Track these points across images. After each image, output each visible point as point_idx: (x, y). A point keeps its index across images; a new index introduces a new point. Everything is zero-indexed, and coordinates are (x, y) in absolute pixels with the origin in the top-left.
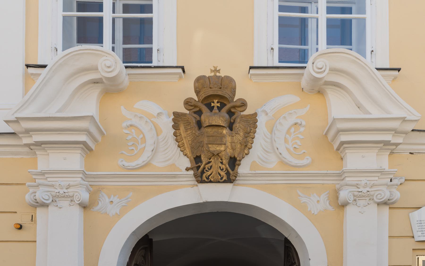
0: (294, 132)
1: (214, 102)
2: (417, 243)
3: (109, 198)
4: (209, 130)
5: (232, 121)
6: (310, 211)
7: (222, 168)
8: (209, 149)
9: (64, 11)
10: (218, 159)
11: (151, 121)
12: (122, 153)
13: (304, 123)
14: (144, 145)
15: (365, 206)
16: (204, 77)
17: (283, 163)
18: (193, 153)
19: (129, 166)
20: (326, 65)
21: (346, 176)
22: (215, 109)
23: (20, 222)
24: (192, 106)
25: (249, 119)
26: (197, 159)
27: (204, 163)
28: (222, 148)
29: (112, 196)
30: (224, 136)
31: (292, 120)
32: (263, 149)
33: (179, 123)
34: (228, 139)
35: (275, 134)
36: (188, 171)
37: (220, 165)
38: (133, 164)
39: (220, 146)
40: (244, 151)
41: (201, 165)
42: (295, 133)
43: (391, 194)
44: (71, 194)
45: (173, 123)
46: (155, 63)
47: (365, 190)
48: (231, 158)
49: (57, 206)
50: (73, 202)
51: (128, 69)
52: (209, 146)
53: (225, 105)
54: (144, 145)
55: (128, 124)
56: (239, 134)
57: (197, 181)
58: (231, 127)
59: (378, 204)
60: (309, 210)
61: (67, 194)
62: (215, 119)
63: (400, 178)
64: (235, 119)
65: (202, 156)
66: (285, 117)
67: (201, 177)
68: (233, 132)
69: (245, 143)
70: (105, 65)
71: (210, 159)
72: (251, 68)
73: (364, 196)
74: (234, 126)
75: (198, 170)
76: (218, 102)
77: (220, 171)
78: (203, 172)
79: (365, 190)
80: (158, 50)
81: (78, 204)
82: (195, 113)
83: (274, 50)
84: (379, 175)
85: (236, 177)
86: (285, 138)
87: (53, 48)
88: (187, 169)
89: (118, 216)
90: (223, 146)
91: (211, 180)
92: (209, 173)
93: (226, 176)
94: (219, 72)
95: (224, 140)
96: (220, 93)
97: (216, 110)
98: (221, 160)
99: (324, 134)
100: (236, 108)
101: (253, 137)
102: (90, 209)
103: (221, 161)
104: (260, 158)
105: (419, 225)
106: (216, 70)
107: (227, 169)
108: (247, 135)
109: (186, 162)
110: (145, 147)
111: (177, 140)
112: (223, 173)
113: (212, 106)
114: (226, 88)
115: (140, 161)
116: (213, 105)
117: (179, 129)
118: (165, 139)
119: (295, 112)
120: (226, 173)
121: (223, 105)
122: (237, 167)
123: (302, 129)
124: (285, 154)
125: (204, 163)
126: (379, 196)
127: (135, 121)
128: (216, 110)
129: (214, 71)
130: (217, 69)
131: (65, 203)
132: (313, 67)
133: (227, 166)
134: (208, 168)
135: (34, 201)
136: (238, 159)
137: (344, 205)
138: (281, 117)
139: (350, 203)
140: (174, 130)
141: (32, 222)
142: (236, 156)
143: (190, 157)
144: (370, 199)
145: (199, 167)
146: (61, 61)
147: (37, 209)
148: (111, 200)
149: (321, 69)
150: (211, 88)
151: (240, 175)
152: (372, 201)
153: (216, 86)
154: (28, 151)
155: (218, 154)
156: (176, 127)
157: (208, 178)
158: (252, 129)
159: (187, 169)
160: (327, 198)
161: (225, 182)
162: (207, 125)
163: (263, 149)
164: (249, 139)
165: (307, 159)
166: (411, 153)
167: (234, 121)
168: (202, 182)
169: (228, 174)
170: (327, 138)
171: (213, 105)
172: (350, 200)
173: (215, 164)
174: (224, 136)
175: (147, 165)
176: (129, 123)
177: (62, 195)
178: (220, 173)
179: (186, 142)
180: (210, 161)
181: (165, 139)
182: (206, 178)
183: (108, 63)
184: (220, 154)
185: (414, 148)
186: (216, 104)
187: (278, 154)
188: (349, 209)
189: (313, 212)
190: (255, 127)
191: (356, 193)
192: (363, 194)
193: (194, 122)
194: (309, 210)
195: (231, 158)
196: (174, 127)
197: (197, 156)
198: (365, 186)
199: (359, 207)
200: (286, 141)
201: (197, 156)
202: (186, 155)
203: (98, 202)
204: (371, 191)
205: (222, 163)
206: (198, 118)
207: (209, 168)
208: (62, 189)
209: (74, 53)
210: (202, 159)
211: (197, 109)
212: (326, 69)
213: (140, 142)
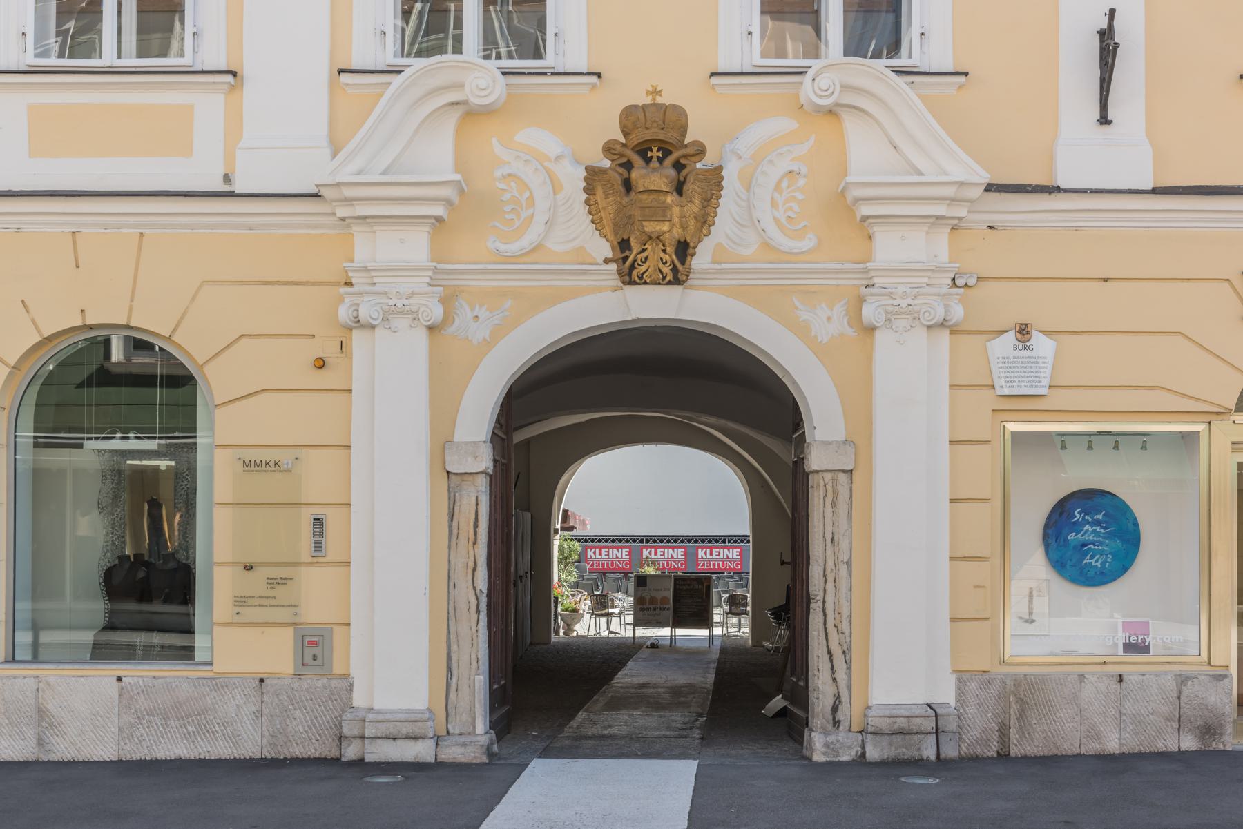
0: (788, 187)
1: (651, 151)
2: (1001, 399)
3: (473, 309)
4: (644, 197)
6: (816, 337)
7: (664, 261)
8: (643, 229)
10: (657, 245)
13: (804, 170)
14: (531, 211)
15: (906, 331)
16: (636, 106)
17: (767, 245)
18: (616, 234)
19: (506, 252)
21: (873, 275)
22: (654, 161)
24: (615, 154)
25: (710, 177)
26: (624, 245)
27: (635, 252)
28: (665, 227)
29: (477, 308)
31: (784, 165)
32: (735, 220)
34: (676, 211)
35: (754, 194)
36: (607, 264)
37: (662, 255)
39: (661, 223)
40: (701, 232)
41: (631, 255)
42: (789, 190)
44: (414, 309)
45: (585, 184)
47: (904, 304)
48: (679, 242)
49: (390, 328)
50: (416, 322)
51: (507, 76)
52: (644, 223)
53: (670, 153)
54: (531, 211)
57: (623, 283)
58: (679, 189)
59: (929, 327)
60: (813, 334)
61: (407, 308)
62: (654, 181)
63: (968, 276)
64: (687, 175)
65: (631, 239)
66: (771, 162)
67: (630, 274)
69: (703, 217)
70: (477, 86)
71: (645, 245)
72: (712, 75)
75: (624, 263)
76: (658, 151)
77: (661, 265)
78: (632, 267)
79: (904, 304)
80: (556, 35)
82: (621, 165)
83: (753, 34)
84: (929, 274)
85: (688, 276)
86: (772, 198)
87: (378, 32)
88: (606, 261)
89: (489, 344)
90: (667, 223)
91: (645, 281)
92: (643, 269)
93: (672, 274)
95: (669, 214)
96: (661, 137)
98: (664, 246)
99: (839, 190)
100: (689, 158)
101: (715, 206)
102: (440, 331)
103: (663, 248)
105: (1001, 365)
106: (656, 92)
107: (673, 262)
108: (705, 204)
109: (604, 249)
111: (590, 212)
112: (666, 270)
113: (649, 156)
114: (671, 128)
115: (524, 243)
116: (650, 154)
117: (595, 194)
118: (567, 202)
120: (671, 270)
121: (667, 153)
122: (689, 258)
123: (801, 182)
124: (774, 232)
125: (635, 252)
126: (927, 314)
128: (654, 163)
129: (652, 93)
130: (658, 90)
131: (401, 323)
132: (813, 86)
133: (674, 257)
134: (641, 260)
135: (354, 319)
136: (691, 245)
137: (871, 329)
139: (878, 327)
140: (586, 196)
141: (342, 355)
142: (688, 240)
143: (612, 241)
144: (914, 319)
146: (407, 82)
147: (355, 332)
148: (475, 314)
149: (827, 90)
150: (647, 128)
151: (695, 271)
153: (655, 125)
154: (336, 222)
156: (589, 190)
157: (641, 278)
158: (714, 194)
159: (606, 261)
160: (844, 312)
161: (669, 283)
162: (641, 190)
163: (735, 220)
164: (710, 210)
165: (810, 239)
166: (990, 227)
167: (685, 179)
168: (632, 283)
169: (675, 270)
170: (845, 197)
171: (650, 154)
172: (877, 322)
173: (654, 253)
175: (538, 248)
176: (506, 171)
177: (400, 311)
178: (661, 268)
179: (608, 214)
180: (645, 248)
181: (567, 202)
182: (638, 277)
183: (482, 83)
185: (994, 219)
186: (655, 153)
187: (761, 231)
188: (878, 335)
190: (720, 188)
191: (890, 309)
192: (902, 310)
193: (620, 182)
194: (813, 334)
195: (679, 242)
196: (586, 190)
197: (623, 239)
199: (896, 332)
200: (774, 204)
201: (623, 239)
202: (605, 237)
203: (454, 318)
204: (915, 305)
205: (664, 251)
206: (626, 175)
207: (643, 260)
208: (400, 299)
209: (428, 68)
210: (632, 244)
211: (624, 160)
212: (834, 90)
213: (524, 205)
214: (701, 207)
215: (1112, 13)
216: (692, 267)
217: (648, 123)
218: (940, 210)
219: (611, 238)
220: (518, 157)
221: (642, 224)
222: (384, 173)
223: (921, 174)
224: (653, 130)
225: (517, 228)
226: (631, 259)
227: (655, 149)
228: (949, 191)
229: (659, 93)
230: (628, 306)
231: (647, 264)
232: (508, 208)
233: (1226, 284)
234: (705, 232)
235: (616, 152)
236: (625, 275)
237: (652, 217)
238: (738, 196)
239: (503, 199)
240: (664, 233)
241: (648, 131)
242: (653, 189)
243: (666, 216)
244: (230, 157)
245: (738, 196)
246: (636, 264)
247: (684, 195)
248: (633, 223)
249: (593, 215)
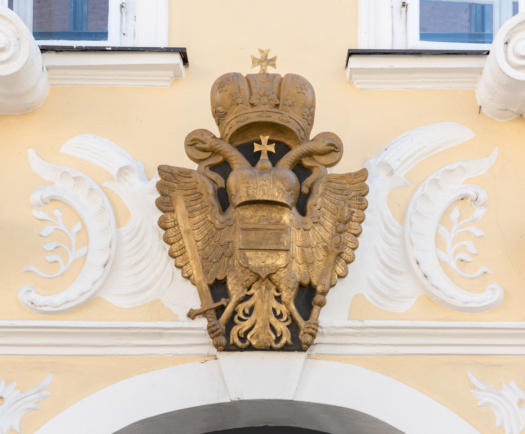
0: (460, 219)
1: (259, 142)
4: (248, 212)
5: (305, 190)
7: (278, 313)
8: (247, 262)
10: (268, 289)
11: (101, 187)
12: (29, 271)
13: (483, 196)
14: (82, 251)
18: (206, 272)
19: (46, 306)
22: (263, 159)
24: (204, 150)
25: (348, 186)
27: (234, 299)
28: (280, 261)
30: (283, 230)
32: (382, 262)
33: (173, 194)
35: (411, 224)
37: (275, 304)
39: (274, 254)
41: (228, 303)
45: (158, 195)
48: (301, 286)
51: (47, 55)
52: (248, 254)
53: (288, 149)
54: (82, 251)
56: (321, 224)
60: (498, 424)
62: (263, 185)
64: (312, 184)
65: (229, 280)
66: (435, 182)
68: (307, 219)
69: (338, 248)
71: (249, 289)
72: (352, 53)
74: (310, 203)
75: (218, 317)
76: (270, 142)
77: (273, 320)
78: (230, 323)
80: (122, 6)
83: (409, 6)
85: (313, 336)
88: (192, 315)
90: (283, 255)
91: (250, 344)
92: (246, 325)
94: (274, 65)
95: (285, 239)
96: (275, 118)
97: (264, 161)
98: (278, 291)
100: (316, 157)
101: (356, 232)
103: (277, 294)
107: (291, 315)
108: (341, 227)
110: (86, 255)
111: (166, 240)
112: (281, 326)
113: (255, 150)
116: (257, 148)
117: (173, 211)
119: (461, 167)
120: (288, 326)
122: (316, 309)
123: (479, 213)
125: (234, 299)
128: (264, 161)
129: (260, 62)
132: (506, 52)
133: (293, 307)
134: (244, 311)
136: (319, 288)
140: (161, 214)
142: (314, 282)
143: (200, 283)
150: (252, 105)
151: (324, 330)
153: (265, 100)
155: (269, 277)
157: (243, 339)
158: (353, 212)
159: (192, 315)
161: (286, 348)
162: (243, 200)
163: (382, 262)
164: (347, 237)
165: (494, 289)
169: (294, 327)
171: (257, 148)
173: (263, 301)
174: (283, 230)
176: (47, 193)
178: (274, 324)
180: (249, 293)
182: (240, 338)
184: (274, 277)
187: (421, 276)
194: (498, 424)
195: (301, 286)
196: (161, 204)
197: (216, 280)
200: (439, 242)
201: (216, 280)
202: (188, 278)
205: (278, 299)
206: (221, 183)
207: (247, 311)
210: (230, 287)
211: (218, 159)
213: (74, 242)
214: (334, 233)
216: (320, 324)
217: (253, 98)
219: (198, 276)
220: (64, 174)
221: (245, 254)
224: (261, 108)
225: (62, 275)
226: (229, 309)
227: (264, 139)
229: (272, 62)
230: (224, 382)
231: (253, 317)
232: (50, 246)
234: (339, 270)
235: (206, 146)
236: (220, 334)
237: (261, 244)
238: (388, 229)
239: (42, 233)
240: (278, 269)
241: (254, 109)
242: (261, 198)
243: (282, 243)
245: (388, 229)
246: (236, 318)
247: (308, 212)
248: (232, 255)
249: (171, 244)
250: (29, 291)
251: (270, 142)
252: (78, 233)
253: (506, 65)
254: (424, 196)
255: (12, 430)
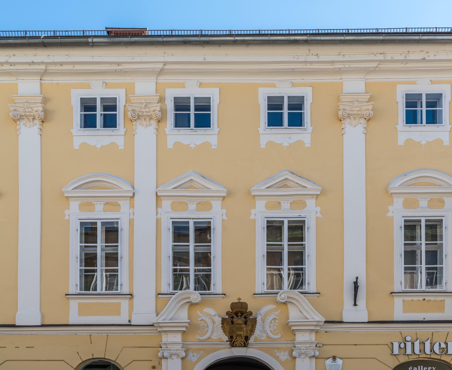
1: (239, 314)
3: (193, 354)
5: (246, 321)
6: (281, 360)
9: (96, 114)
10: (240, 337)
11: (210, 317)
12: (198, 333)
13: (278, 318)
17: (268, 337)
18: (229, 334)
20: (285, 297)
23: (154, 365)
24: (229, 315)
26: (231, 337)
27: (234, 339)
28: (242, 333)
30: (243, 328)
31: (273, 317)
33: (224, 322)
34: (245, 329)
35: (265, 324)
37: (241, 340)
38: (203, 338)
43: (314, 353)
44: (178, 354)
46: (212, 291)
52: (237, 332)
53: (243, 314)
55: (201, 319)
56: (249, 326)
58: (246, 323)
59: (310, 357)
60: (280, 359)
61: (176, 353)
65: (233, 336)
66: (269, 316)
68: (247, 326)
69: (252, 330)
70: (194, 298)
72: (254, 294)
73: (303, 354)
74: (247, 323)
77: (241, 342)
78: (234, 343)
81: (181, 358)
82: (231, 317)
84: (310, 344)
88: (227, 341)
90: (243, 332)
92: (236, 343)
94: (241, 300)
97: (239, 317)
98: (242, 337)
99: (287, 323)
104: (258, 335)
106: (239, 299)
107: (244, 341)
109: (226, 338)
110: (208, 330)
111: (223, 329)
112: (242, 343)
115: (206, 337)
116: (238, 315)
118: (217, 326)
119: (274, 313)
122: (248, 341)
123: (277, 321)
126: (309, 354)
127: (204, 318)
128: (239, 317)
133: (244, 340)
136: (249, 337)
137: (295, 358)
138: (268, 316)
142: (248, 336)
145: (232, 341)
148: (193, 355)
152: (307, 356)
155: (240, 335)
157: (236, 345)
159: (227, 341)
161: (243, 347)
164: (253, 328)
165: (279, 335)
166: (326, 332)
167: (247, 320)
168: (233, 347)
169: (244, 343)
174: (243, 328)
175: (209, 338)
181: (217, 326)
183: (195, 297)
184: (241, 335)
185: (327, 330)
189: (282, 360)
191: (300, 353)
193: (230, 322)
194: (280, 359)
195: (246, 336)
196: (222, 324)
198: (304, 349)
200: (270, 326)
204: (306, 352)
205: (242, 339)
210: (234, 337)
211: (231, 316)
213: (206, 327)
215: (357, 278)
218: (313, 328)
222: (170, 320)
223: (308, 319)
227: (239, 313)
228: (315, 323)
229: (241, 299)
231: (237, 342)
232: (202, 328)
233: (387, 346)
238: (261, 324)
240: (242, 334)
244: (130, 315)
245: (261, 324)
250: (198, 336)
251: (240, 314)
252: (207, 326)
253: (280, 299)
254: (267, 319)
255: (196, 361)
